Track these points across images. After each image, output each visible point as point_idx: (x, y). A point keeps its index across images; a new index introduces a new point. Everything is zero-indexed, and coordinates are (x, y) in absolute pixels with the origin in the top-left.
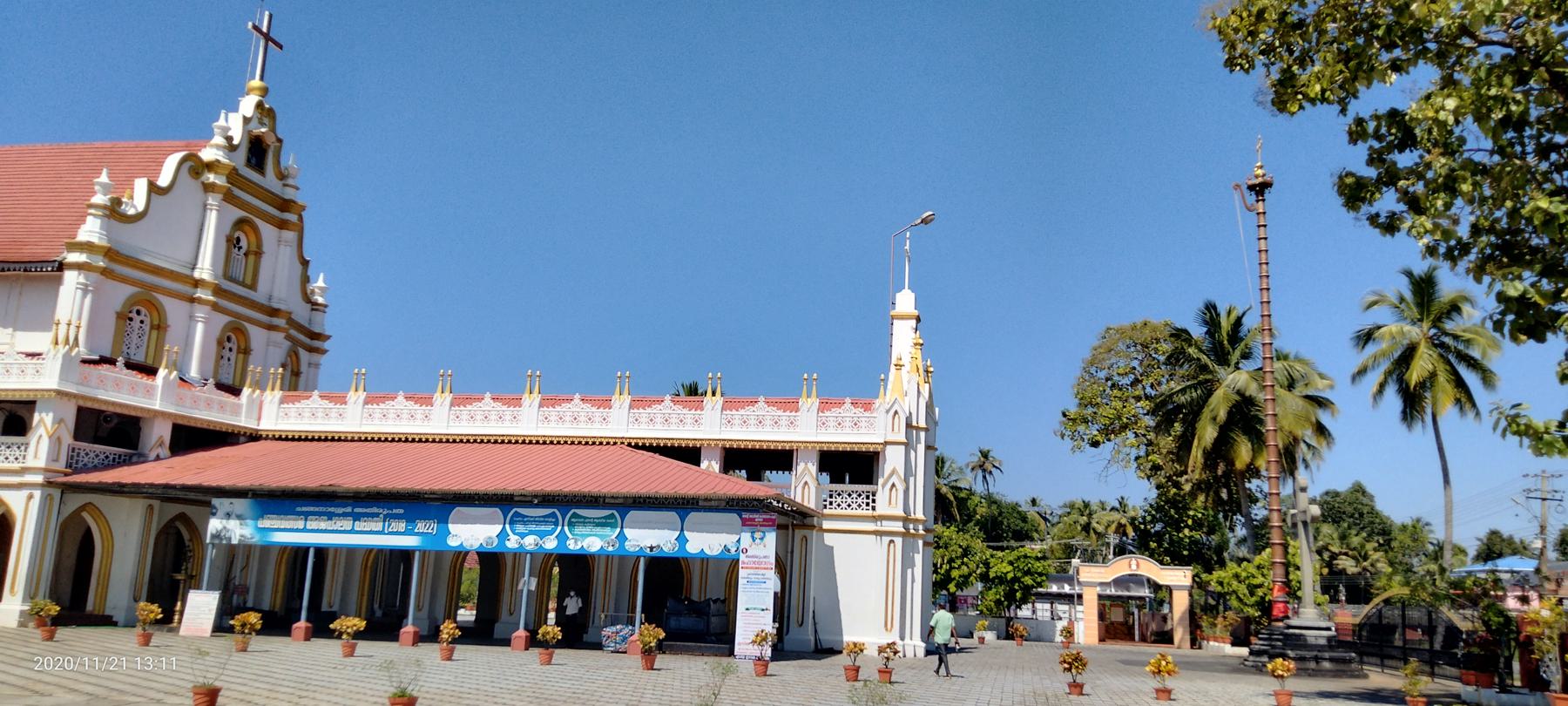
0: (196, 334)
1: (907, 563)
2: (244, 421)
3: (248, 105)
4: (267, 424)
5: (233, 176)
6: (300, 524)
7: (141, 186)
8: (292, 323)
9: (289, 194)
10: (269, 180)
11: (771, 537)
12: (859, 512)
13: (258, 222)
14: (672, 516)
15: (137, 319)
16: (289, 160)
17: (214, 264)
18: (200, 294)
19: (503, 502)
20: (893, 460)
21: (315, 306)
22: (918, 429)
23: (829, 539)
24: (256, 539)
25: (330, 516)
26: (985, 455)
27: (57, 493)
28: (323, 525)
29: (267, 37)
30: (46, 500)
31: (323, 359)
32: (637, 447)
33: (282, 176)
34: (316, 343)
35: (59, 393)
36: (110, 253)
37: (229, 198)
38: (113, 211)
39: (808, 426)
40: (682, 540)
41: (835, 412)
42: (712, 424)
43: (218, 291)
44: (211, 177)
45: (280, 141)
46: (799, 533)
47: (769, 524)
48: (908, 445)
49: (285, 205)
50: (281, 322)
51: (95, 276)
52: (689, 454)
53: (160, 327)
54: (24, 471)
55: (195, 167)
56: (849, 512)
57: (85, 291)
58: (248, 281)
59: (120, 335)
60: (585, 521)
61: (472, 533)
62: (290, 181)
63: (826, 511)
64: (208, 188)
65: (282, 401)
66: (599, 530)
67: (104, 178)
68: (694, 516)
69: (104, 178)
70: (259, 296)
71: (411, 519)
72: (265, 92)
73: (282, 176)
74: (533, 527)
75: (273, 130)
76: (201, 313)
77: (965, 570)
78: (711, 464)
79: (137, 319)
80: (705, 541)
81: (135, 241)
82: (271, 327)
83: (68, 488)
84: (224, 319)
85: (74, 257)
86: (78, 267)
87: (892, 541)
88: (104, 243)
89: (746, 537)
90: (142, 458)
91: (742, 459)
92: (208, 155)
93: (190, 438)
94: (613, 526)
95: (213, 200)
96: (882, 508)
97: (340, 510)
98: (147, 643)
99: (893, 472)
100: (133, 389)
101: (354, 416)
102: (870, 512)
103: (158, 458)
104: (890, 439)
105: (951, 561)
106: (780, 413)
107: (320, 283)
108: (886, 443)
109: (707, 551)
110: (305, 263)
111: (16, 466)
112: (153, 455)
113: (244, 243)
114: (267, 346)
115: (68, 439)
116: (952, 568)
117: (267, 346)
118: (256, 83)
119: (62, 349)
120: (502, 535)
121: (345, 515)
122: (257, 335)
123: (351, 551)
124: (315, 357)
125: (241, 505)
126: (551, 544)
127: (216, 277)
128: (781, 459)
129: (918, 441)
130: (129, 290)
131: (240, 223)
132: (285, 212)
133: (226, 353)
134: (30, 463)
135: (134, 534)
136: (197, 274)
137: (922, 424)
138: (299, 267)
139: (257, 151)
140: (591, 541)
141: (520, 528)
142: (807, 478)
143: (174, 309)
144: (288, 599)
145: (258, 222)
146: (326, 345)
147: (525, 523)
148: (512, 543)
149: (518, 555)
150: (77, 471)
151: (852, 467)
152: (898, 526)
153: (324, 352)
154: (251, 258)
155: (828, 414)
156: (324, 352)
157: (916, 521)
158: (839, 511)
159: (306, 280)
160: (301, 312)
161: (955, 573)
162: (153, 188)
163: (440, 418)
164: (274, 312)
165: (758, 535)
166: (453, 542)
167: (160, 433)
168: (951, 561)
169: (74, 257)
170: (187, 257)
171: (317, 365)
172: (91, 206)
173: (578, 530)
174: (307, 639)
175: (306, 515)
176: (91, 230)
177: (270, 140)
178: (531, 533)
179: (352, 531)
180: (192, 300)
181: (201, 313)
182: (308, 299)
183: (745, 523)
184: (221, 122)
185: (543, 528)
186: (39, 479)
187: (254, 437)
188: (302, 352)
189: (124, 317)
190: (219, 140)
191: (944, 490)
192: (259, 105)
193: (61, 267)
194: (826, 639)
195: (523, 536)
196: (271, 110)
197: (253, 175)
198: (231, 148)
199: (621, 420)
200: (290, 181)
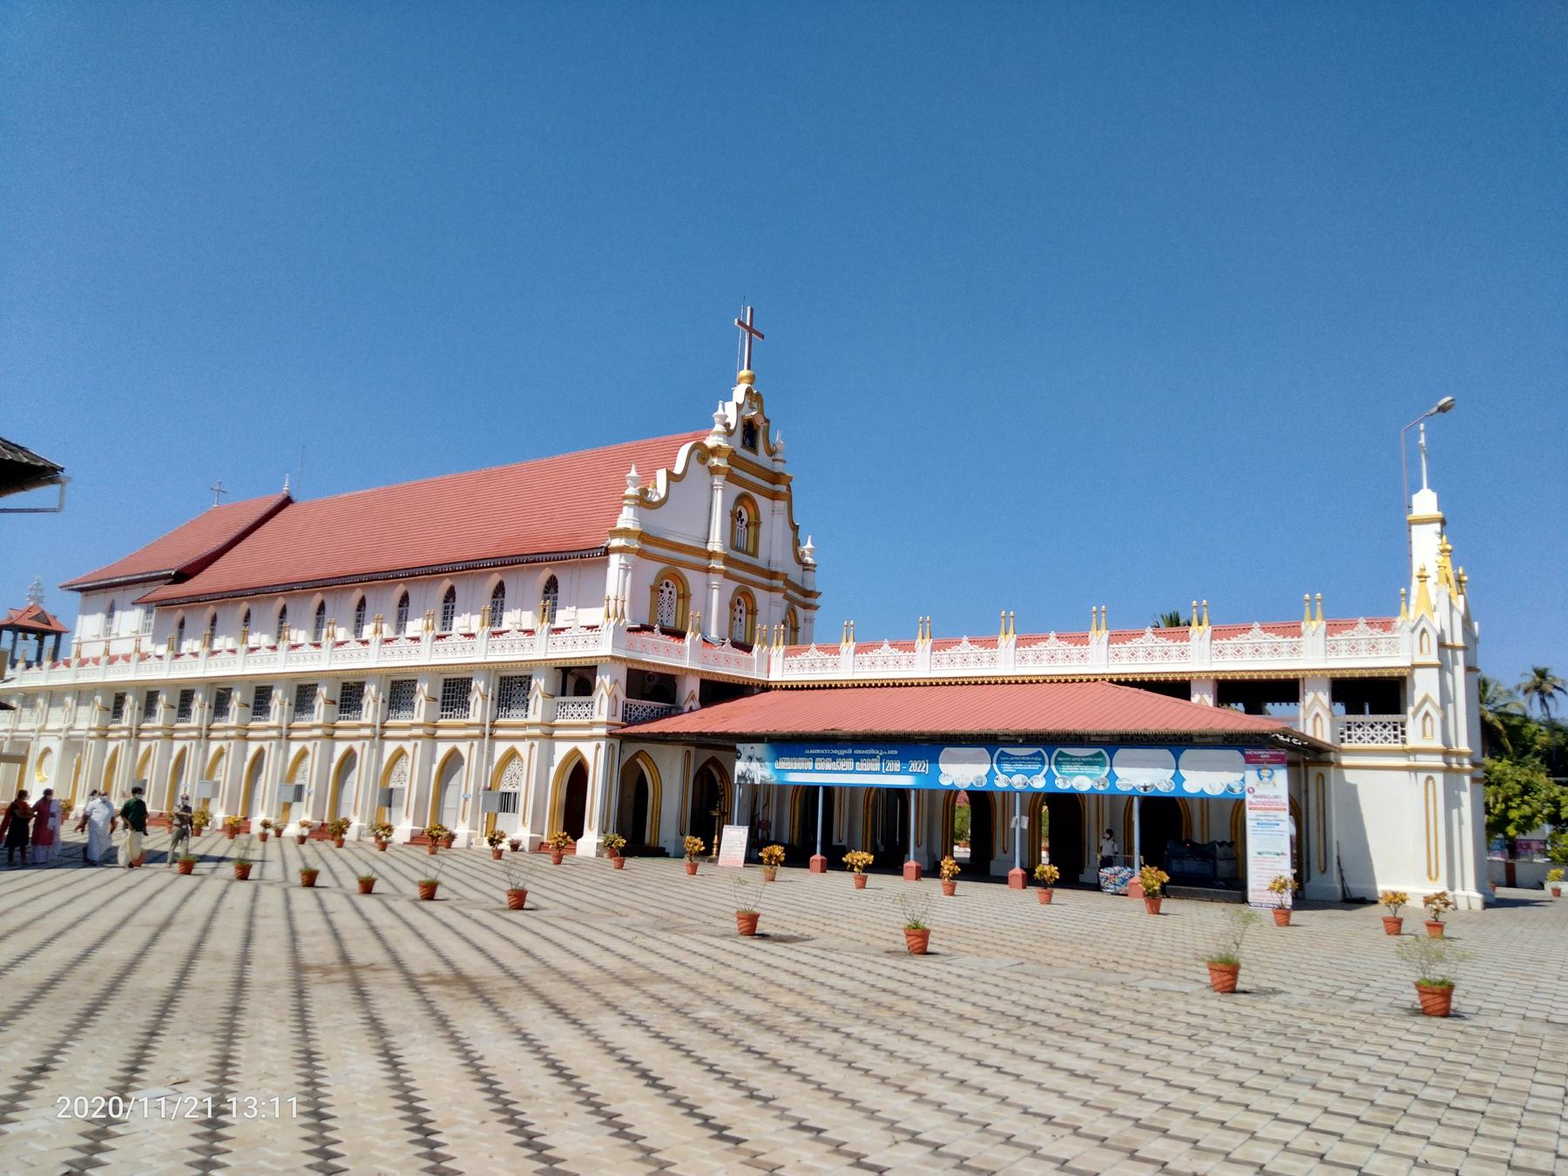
0: (712, 599)
1: (1452, 802)
2: (756, 675)
3: (739, 393)
4: (776, 676)
5: (733, 458)
6: (809, 765)
7: (661, 475)
8: (788, 583)
9: (779, 467)
10: (762, 458)
11: (1281, 776)
12: (1386, 745)
13: (755, 496)
14: (1165, 754)
15: (667, 590)
16: (777, 438)
17: (722, 538)
18: (717, 564)
19: (989, 742)
20: (1424, 686)
21: (806, 567)
22: (1453, 648)
23: (1350, 776)
24: (774, 780)
25: (834, 758)
26: (1542, 674)
27: (617, 743)
28: (829, 765)
29: (751, 330)
30: (610, 748)
31: (817, 614)
32: (1119, 683)
33: (771, 453)
34: (810, 600)
35: (612, 657)
36: (643, 536)
37: (731, 477)
38: (643, 501)
39: (1314, 652)
40: (1178, 779)
41: (1347, 634)
42: (1202, 655)
43: (727, 560)
44: (715, 461)
45: (767, 421)
46: (1313, 771)
47: (1278, 761)
48: (1443, 668)
49: (776, 478)
50: (779, 583)
51: (632, 557)
52: (1178, 688)
53: (685, 596)
54: (592, 725)
55: (702, 454)
56: (1373, 745)
57: (626, 571)
58: (751, 549)
59: (655, 606)
60: (1072, 760)
61: (962, 772)
62: (778, 456)
63: (1344, 745)
64: (714, 471)
65: (786, 655)
66: (1087, 769)
67: (633, 473)
68: (1189, 754)
69: (633, 473)
70: (760, 562)
71: (904, 760)
72: (752, 379)
73: (771, 453)
74: (1020, 766)
75: (761, 412)
76: (715, 581)
77: (1526, 810)
78: (1203, 698)
79: (667, 590)
80: (1205, 779)
81: (661, 523)
82: (771, 589)
83: (626, 739)
84: (732, 585)
85: (616, 542)
86: (620, 550)
87: (1429, 778)
88: (637, 528)
89: (1251, 775)
90: (673, 710)
91: (1230, 690)
92: (711, 442)
93: (718, 691)
94: (1102, 765)
95: (718, 481)
96: (1414, 739)
97: (842, 752)
98: (863, 886)
99: (1426, 699)
100: (668, 650)
101: (847, 666)
102: (1400, 746)
103: (691, 710)
104: (1418, 661)
105: (1507, 799)
106: (1280, 639)
107: (809, 545)
108: (1414, 667)
109: (1209, 792)
110: (795, 528)
111: (586, 721)
112: (687, 708)
113: (745, 516)
114: (770, 605)
115: (622, 697)
116: (1508, 808)
117: (770, 605)
118: (745, 372)
119: (613, 622)
120: (991, 775)
121: (846, 756)
122: (761, 596)
123: (854, 789)
124: (809, 613)
125: (759, 749)
126: (1039, 783)
127: (725, 548)
128: (1286, 689)
129: (1455, 662)
130: (660, 566)
131: (741, 499)
132: (776, 484)
133: (738, 615)
134: (597, 718)
135: (676, 781)
136: (710, 548)
137: (1459, 641)
138: (791, 532)
139: (750, 432)
140: (1080, 780)
141: (1007, 767)
142: (1318, 710)
143: (693, 578)
144: (803, 833)
145: (755, 496)
146: (818, 601)
147: (1011, 762)
148: (1001, 782)
149: (1007, 795)
150: (630, 724)
151: (1374, 696)
152: (1437, 761)
153: (816, 608)
154: (752, 529)
155: (1338, 637)
156: (816, 608)
157: (1459, 754)
158: (1360, 745)
159: (797, 543)
160: (795, 573)
161: (1513, 814)
162: (671, 477)
163: (923, 663)
164: (773, 575)
165: (1265, 773)
166: (945, 782)
167: (691, 687)
168: (1507, 799)
169: (616, 542)
170: (701, 533)
171: (811, 621)
172: (625, 498)
173: (1066, 769)
174: (823, 871)
175: (814, 757)
176: (627, 518)
177: (760, 421)
178: (1019, 772)
179: (854, 772)
180: (708, 570)
181: (715, 581)
182: (799, 560)
183: (1249, 760)
184: (720, 411)
185: (1030, 767)
186: (603, 731)
187: (766, 688)
188: (799, 610)
189: (656, 590)
190: (719, 427)
191: (1490, 717)
192: (748, 392)
193: (607, 551)
194: (1356, 887)
195: (1010, 775)
196: (758, 395)
197: (748, 455)
198: (729, 433)
199: (1100, 656)
200: (778, 456)
